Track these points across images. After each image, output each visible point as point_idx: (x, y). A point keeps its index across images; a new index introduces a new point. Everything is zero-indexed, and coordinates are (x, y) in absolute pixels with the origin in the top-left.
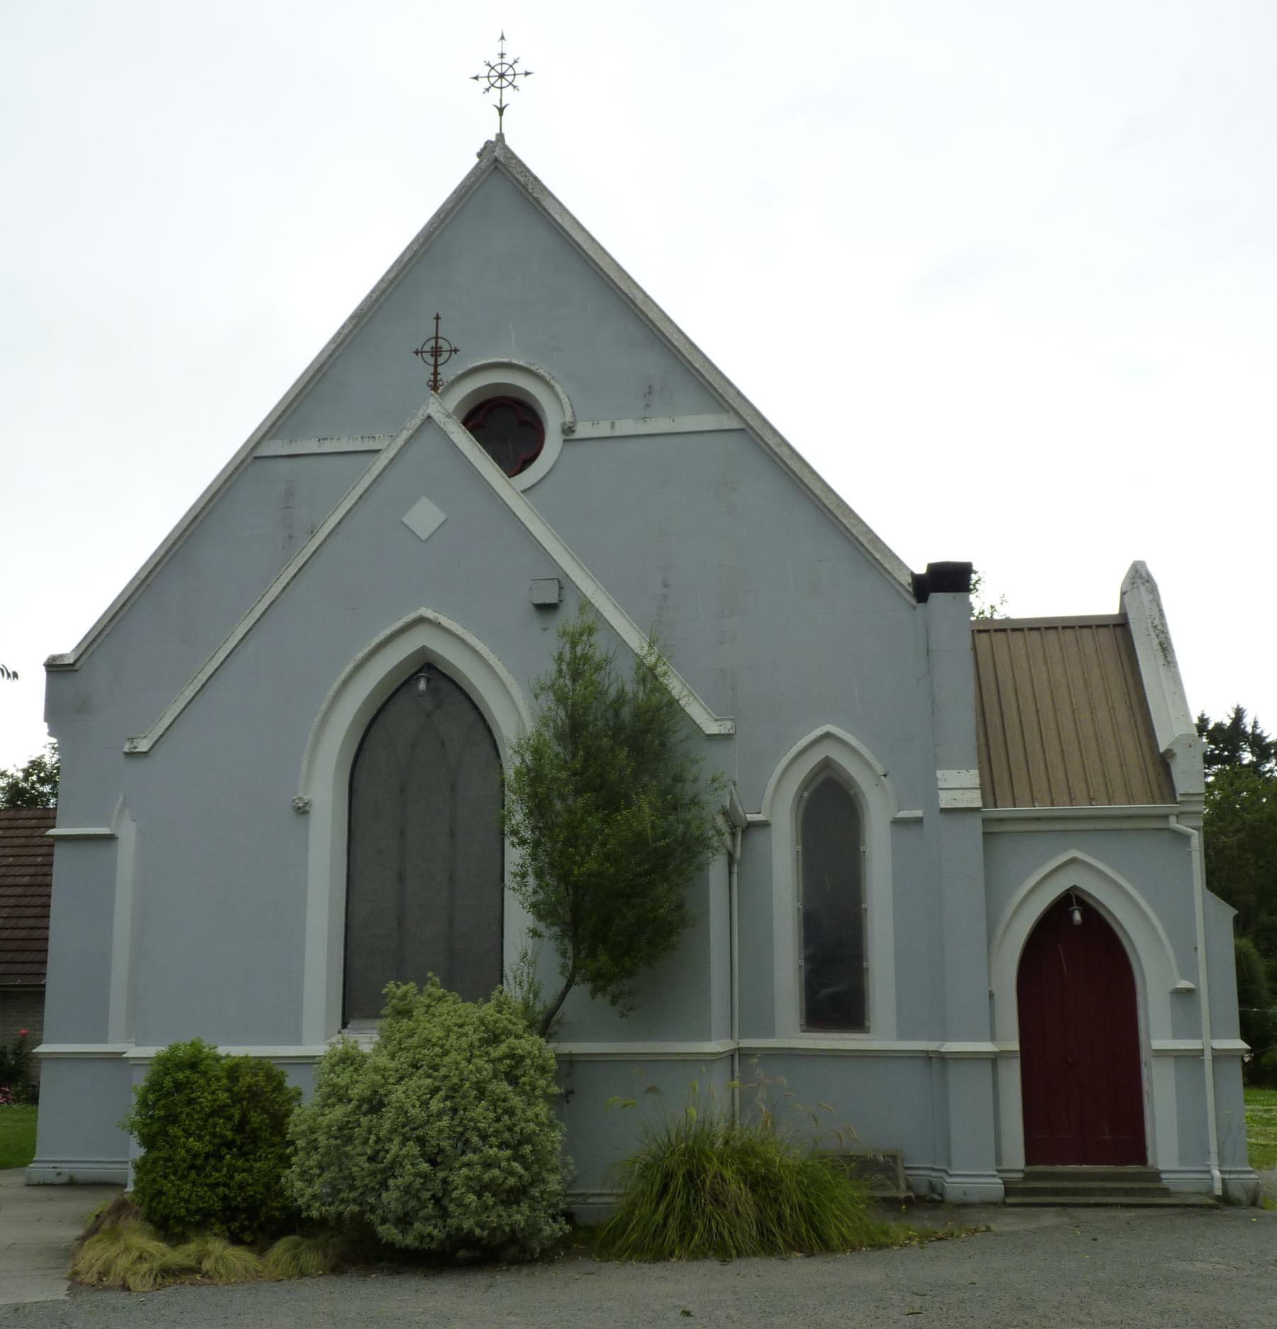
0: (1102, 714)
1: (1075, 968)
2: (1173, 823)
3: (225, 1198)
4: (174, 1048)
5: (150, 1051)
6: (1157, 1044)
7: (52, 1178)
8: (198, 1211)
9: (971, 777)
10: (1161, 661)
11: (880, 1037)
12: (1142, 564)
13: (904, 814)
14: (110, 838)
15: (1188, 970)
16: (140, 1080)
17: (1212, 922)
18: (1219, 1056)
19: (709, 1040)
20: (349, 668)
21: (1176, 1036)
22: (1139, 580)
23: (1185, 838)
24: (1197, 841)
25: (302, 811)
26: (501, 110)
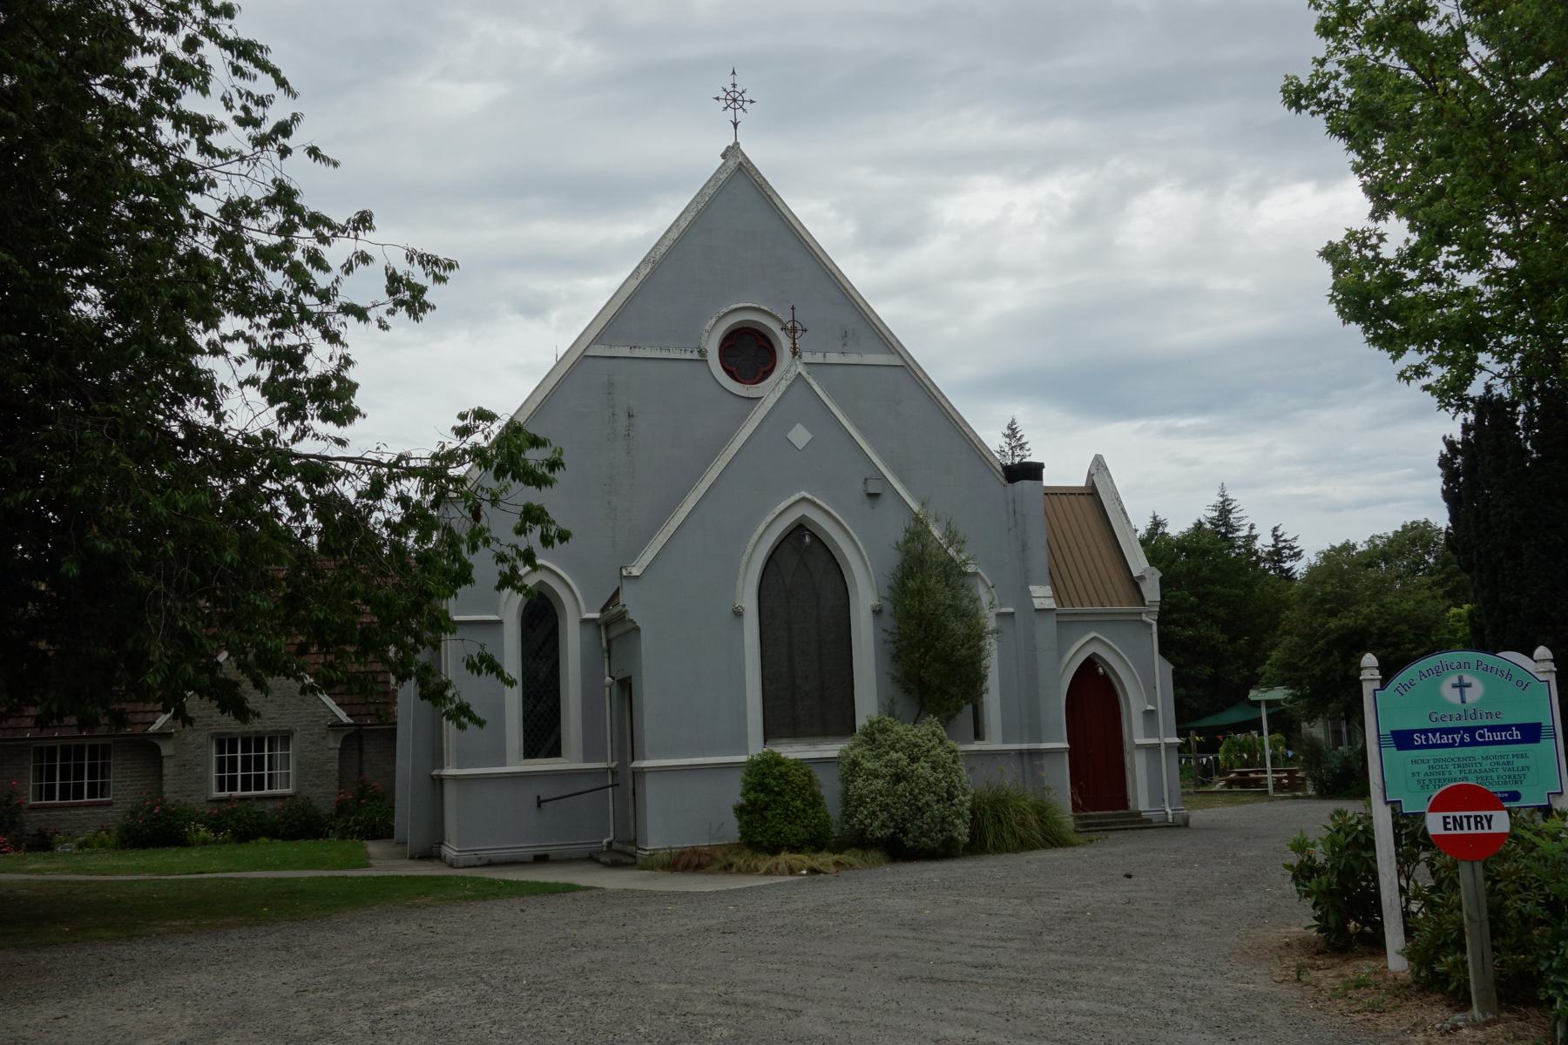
0: (1094, 552)
1: (1093, 695)
2: (1144, 617)
6: (1137, 741)
7: (475, 862)
9: (1047, 590)
11: (993, 742)
13: (1003, 610)
14: (499, 623)
15: (1152, 700)
17: (1162, 671)
18: (1168, 746)
21: (1146, 736)
22: (1099, 463)
23: (1150, 625)
24: (1155, 628)
25: (738, 614)
26: (736, 125)
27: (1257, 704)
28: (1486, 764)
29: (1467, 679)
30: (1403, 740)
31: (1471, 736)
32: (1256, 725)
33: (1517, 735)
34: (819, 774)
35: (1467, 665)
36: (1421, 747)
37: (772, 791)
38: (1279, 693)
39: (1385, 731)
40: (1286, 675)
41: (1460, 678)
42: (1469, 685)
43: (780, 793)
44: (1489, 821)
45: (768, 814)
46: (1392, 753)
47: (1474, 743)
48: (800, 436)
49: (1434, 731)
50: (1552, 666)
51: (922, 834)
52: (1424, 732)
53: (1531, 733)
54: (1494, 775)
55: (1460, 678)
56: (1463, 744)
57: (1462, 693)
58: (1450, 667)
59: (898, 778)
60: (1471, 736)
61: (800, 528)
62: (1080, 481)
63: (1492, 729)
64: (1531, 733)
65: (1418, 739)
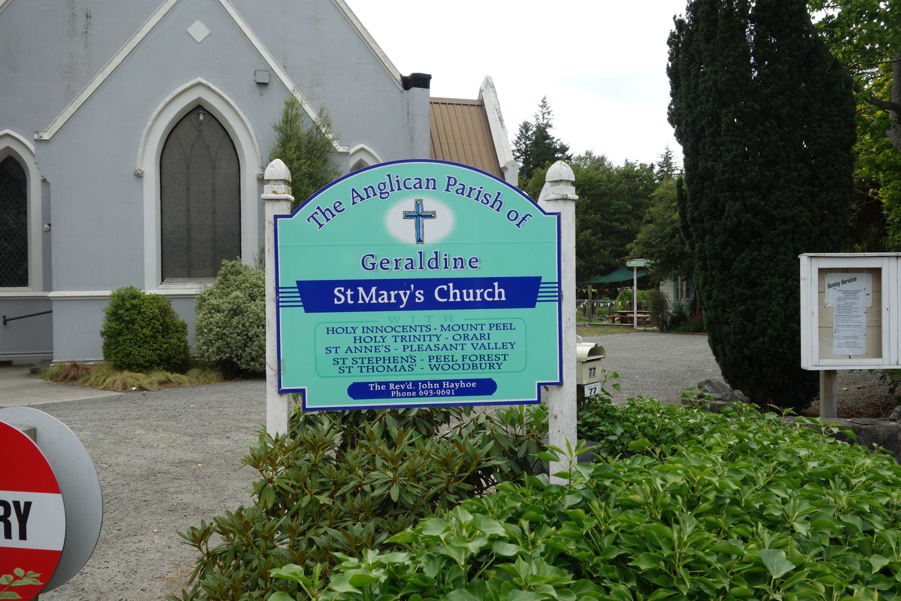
0: (475, 147)
3: (159, 355)
4: (118, 290)
5: (108, 293)
8: (148, 361)
10: (500, 126)
12: (491, 78)
16: (107, 305)
19: (51, 291)
20: (161, 106)
22: (489, 84)
25: (139, 176)
27: (631, 269)
28: (447, 338)
29: (427, 207)
30: (317, 296)
31: (428, 294)
32: (630, 283)
33: (500, 293)
34: (175, 306)
35: (431, 184)
36: (345, 308)
37: (124, 321)
38: (641, 263)
39: (289, 280)
40: (645, 250)
41: (419, 203)
42: (431, 216)
43: (133, 322)
44: (23, 519)
45: (121, 339)
46: (297, 317)
47: (430, 304)
48: (199, 31)
49: (367, 285)
50: (571, 192)
51: (253, 359)
52: (352, 285)
53: (523, 292)
54: (458, 354)
55: (419, 203)
56: (412, 305)
57: (418, 227)
58: (403, 185)
59: (236, 312)
60: (428, 294)
61: (199, 108)
62: (474, 96)
63: (461, 284)
64: (523, 292)
65: (341, 296)
